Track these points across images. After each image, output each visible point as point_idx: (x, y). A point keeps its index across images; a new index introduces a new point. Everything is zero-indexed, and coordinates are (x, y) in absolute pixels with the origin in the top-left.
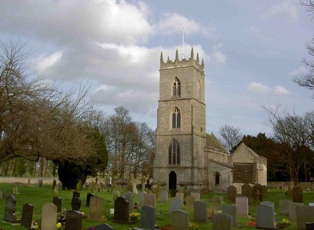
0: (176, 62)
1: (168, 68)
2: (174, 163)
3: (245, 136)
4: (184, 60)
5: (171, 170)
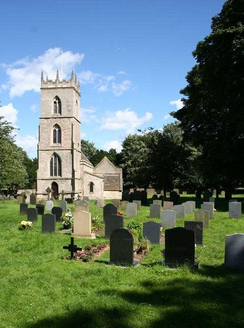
0: (58, 82)
3: (98, 150)
5: (53, 181)
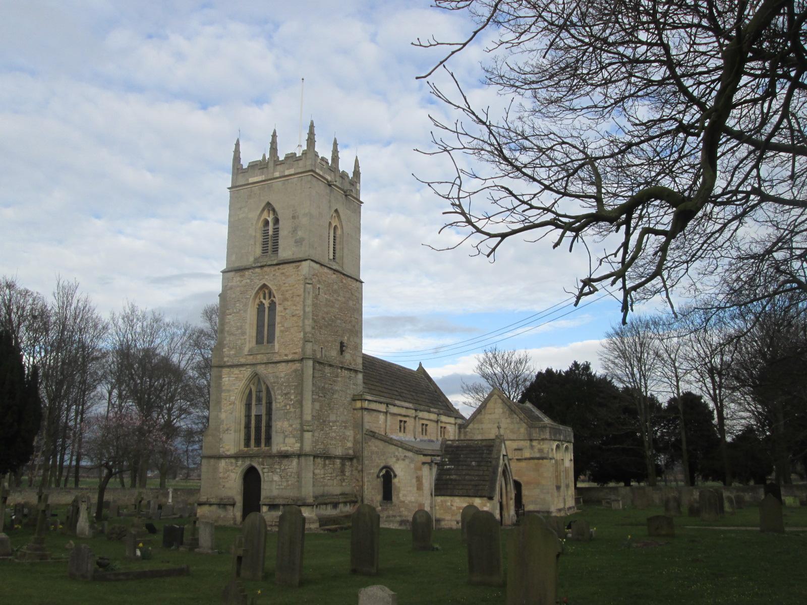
1: (251, 180)
2: (258, 443)
4: (291, 157)
5: (248, 463)
